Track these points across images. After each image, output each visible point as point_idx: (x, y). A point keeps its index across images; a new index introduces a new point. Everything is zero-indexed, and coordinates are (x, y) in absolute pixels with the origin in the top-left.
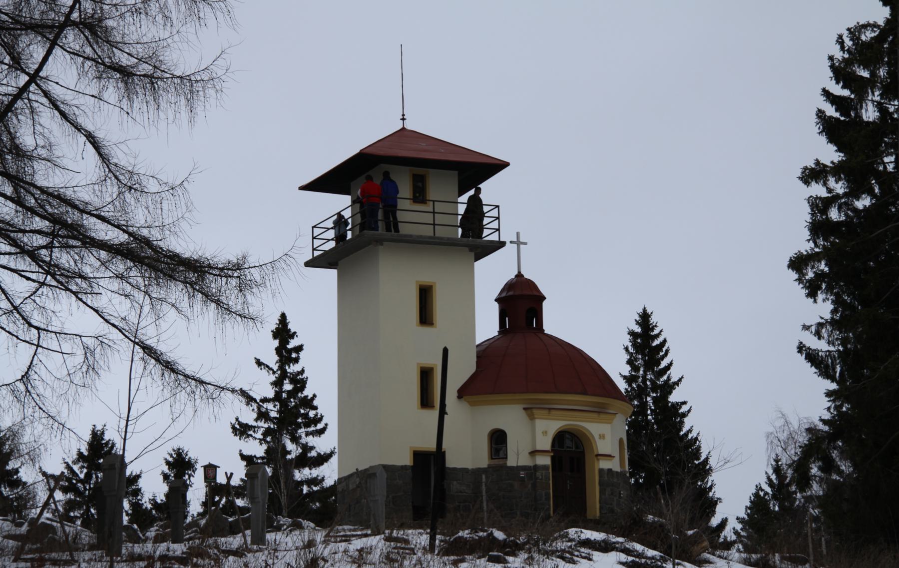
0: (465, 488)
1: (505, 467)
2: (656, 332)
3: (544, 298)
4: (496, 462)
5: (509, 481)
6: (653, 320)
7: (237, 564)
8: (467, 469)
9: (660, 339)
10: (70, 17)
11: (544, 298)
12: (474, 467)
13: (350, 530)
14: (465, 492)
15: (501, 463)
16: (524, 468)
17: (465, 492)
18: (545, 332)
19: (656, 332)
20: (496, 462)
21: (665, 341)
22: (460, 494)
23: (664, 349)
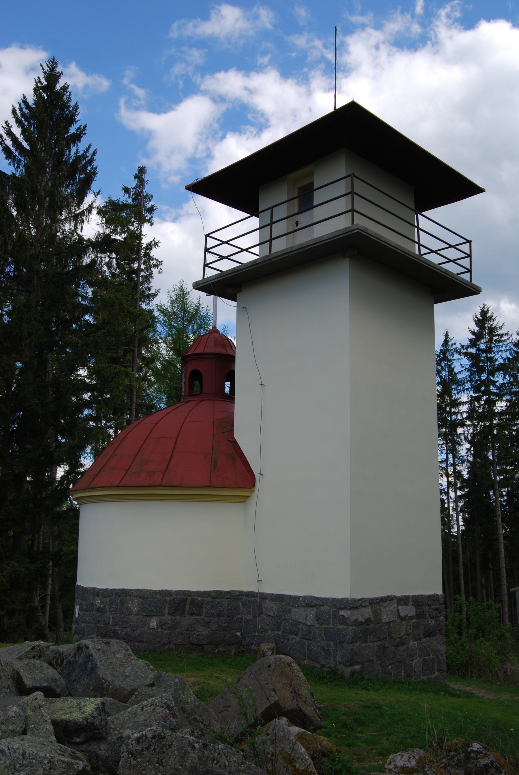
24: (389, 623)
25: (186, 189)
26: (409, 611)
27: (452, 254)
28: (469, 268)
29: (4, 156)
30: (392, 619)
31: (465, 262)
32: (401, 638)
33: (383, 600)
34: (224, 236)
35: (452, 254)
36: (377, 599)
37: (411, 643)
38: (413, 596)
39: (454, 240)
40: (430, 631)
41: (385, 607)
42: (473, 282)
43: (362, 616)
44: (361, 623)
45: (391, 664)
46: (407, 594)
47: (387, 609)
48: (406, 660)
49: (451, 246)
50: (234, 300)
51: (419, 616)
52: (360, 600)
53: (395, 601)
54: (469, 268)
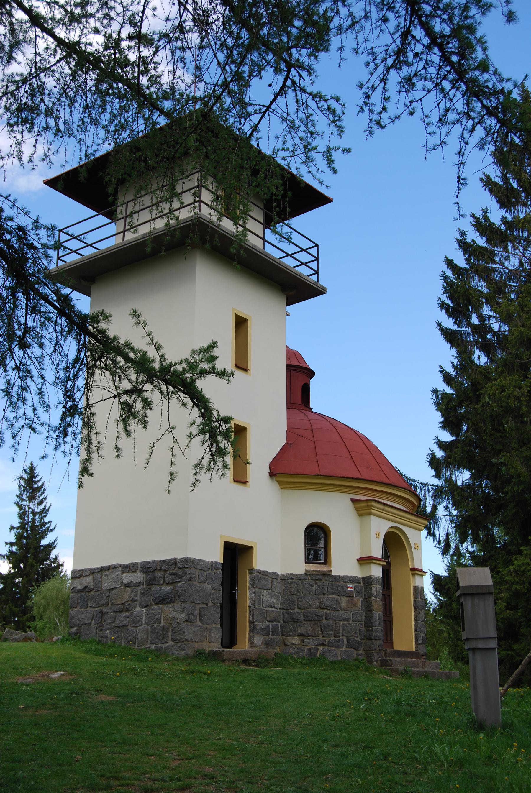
0: (275, 601)
1: (327, 575)
2: (36, 479)
3: (311, 374)
4: (312, 567)
5: (334, 596)
6: (37, 471)
7: (145, 669)
8: (275, 574)
9: (40, 484)
10: (453, 54)
11: (311, 374)
12: (285, 573)
13: (415, 665)
14: (274, 607)
15: (325, 570)
16: (353, 580)
17: (274, 607)
18: (313, 410)
19: (36, 479)
20: (312, 567)
21: (43, 484)
22: (270, 609)
23: (42, 490)
24: (110, 590)
25: (44, 183)
26: (138, 577)
27: (304, 257)
28: (316, 270)
29: (455, 262)
30: (114, 586)
31: (314, 265)
32: (124, 604)
33: (102, 570)
34: (76, 231)
35: (304, 257)
36: (98, 568)
37: (138, 609)
38: (141, 563)
39: (306, 244)
40: (161, 597)
41: (107, 575)
42: (320, 282)
43: (81, 584)
44: (80, 591)
45: (108, 629)
46: (137, 561)
47: (109, 577)
48: (127, 626)
49: (302, 250)
50: (89, 295)
51: (150, 583)
52: (80, 571)
53: (120, 569)
54: (316, 270)
